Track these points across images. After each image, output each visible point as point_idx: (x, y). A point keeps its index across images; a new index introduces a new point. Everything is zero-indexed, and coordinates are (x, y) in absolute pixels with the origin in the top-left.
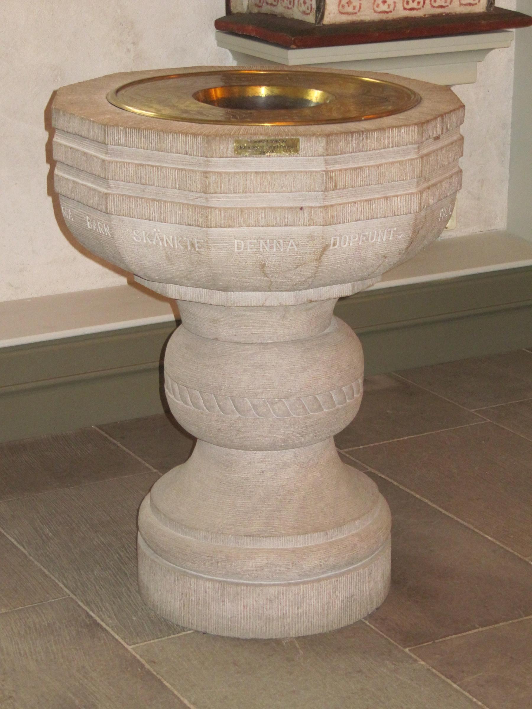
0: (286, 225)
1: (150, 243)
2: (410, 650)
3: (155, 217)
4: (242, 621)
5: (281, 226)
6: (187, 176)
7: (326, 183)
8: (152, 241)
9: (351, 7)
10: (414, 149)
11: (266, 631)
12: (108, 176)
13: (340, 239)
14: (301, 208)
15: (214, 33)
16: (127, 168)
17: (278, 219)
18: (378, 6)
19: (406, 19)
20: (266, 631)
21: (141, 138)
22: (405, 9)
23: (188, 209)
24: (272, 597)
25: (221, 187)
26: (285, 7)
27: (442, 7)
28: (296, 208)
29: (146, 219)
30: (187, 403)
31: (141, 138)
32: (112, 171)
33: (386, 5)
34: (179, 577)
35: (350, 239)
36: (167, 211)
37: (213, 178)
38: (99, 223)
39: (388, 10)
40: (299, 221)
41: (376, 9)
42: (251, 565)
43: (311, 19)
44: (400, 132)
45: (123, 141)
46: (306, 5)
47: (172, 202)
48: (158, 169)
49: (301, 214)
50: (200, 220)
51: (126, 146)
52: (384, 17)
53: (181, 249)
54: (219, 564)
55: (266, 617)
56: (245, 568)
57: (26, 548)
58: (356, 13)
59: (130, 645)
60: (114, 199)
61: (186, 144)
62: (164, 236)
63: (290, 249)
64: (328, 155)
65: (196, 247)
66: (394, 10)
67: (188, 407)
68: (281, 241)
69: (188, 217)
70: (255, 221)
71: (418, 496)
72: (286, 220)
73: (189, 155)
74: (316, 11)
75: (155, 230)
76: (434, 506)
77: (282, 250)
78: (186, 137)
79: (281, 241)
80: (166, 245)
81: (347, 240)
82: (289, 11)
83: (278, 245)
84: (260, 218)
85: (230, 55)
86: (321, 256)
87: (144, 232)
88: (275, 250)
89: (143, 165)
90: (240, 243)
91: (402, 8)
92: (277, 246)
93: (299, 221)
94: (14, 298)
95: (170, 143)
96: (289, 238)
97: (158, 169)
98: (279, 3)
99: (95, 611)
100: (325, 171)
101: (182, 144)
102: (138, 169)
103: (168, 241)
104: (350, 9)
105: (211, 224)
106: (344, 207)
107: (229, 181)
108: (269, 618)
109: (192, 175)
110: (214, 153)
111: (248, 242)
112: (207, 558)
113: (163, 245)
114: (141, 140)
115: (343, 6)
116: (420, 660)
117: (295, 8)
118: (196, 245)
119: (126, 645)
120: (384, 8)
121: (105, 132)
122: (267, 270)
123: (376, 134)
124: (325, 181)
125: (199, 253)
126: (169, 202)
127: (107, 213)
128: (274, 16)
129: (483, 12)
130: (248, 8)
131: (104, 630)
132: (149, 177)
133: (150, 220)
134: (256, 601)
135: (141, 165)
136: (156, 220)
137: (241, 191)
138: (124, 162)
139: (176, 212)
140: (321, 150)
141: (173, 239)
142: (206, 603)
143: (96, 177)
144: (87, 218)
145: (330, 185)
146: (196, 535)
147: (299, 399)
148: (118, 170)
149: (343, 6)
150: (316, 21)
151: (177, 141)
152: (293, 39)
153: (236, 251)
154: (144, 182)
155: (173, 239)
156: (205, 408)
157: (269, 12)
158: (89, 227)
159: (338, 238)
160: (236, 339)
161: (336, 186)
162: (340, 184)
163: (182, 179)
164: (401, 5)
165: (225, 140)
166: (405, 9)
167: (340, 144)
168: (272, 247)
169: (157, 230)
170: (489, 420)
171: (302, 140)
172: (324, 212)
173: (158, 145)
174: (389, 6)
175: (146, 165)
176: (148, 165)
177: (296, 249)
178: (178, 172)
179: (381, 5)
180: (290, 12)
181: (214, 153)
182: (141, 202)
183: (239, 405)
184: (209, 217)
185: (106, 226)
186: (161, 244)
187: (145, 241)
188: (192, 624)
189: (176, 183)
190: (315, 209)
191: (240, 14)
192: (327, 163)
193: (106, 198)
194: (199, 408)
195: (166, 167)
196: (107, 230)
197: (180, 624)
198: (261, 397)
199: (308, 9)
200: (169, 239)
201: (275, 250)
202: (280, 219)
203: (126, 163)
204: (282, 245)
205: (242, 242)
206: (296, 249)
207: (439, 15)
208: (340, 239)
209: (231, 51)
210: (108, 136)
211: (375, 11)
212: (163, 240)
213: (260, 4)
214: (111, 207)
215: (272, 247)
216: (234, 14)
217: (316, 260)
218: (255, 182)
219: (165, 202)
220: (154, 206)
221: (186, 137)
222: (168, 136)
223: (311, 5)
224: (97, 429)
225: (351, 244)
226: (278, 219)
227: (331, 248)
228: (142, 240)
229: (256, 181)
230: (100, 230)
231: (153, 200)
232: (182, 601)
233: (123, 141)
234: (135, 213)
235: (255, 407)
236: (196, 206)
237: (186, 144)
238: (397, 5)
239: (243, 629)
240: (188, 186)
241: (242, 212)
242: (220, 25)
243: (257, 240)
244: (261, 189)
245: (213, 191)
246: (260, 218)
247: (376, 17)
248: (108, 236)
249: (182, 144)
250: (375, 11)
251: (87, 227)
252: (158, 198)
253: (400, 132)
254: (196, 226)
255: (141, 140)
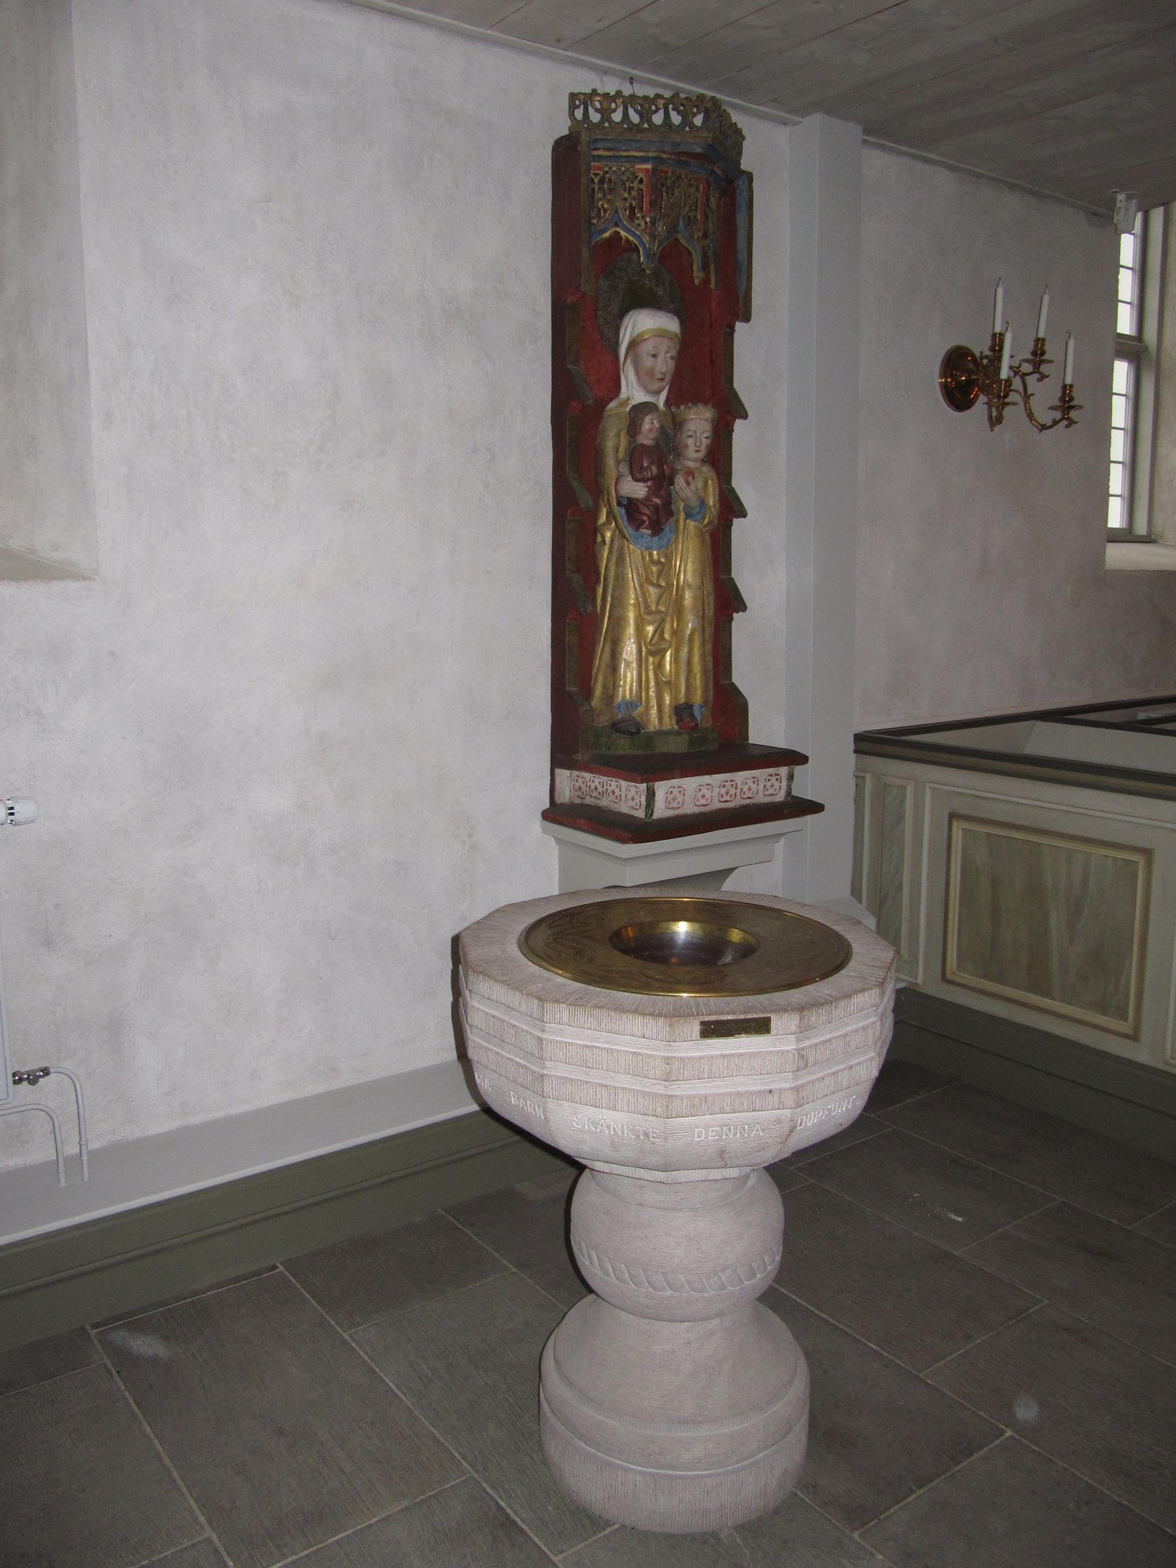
0: (753, 1111)
1: (594, 1129)
2: (859, 1536)
3: (602, 1103)
4: (677, 1516)
5: (748, 1112)
6: (644, 1061)
7: (798, 1063)
8: (596, 1128)
9: (676, 802)
10: (874, 1011)
11: (703, 1525)
12: (546, 1056)
13: (807, 1118)
14: (770, 1091)
15: (539, 822)
16: (569, 1049)
17: (746, 1104)
18: (698, 800)
19: (721, 810)
20: (703, 1525)
21: (588, 1017)
22: (720, 802)
23: (644, 1097)
24: (709, 1488)
25: (684, 1074)
26: (611, 801)
27: (750, 798)
28: (765, 1091)
29: (591, 1106)
30: (608, 1276)
31: (588, 1017)
32: (551, 1051)
33: (705, 799)
34: (603, 1467)
35: (815, 1116)
36: (618, 1098)
37: (676, 1065)
38: (528, 1102)
39: (706, 803)
40: (768, 1104)
41: (697, 803)
42: (687, 1456)
43: (640, 814)
44: (864, 996)
45: (565, 1019)
46: (635, 801)
47: (623, 1089)
48: (608, 1052)
49: (769, 1098)
50: (659, 1109)
51: (569, 1026)
52: (702, 809)
53: (631, 1138)
54: (652, 1457)
55: (703, 1509)
56: (681, 1460)
57: (408, 1395)
58: (680, 808)
59: (556, 1555)
60: (552, 1081)
61: (644, 1026)
62: (612, 1123)
63: (755, 1134)
64: (800, 1033)
65: (651, 1136)
66: (711, 803)
67: (609, 1279)
68: (746, 1126)
69: (644, 1106)
70: (720, 1108)
71: (783, 1290)
72: (754, 1105)
73: (647, 1038)
74: (646, 807)
75: (601, 1116)
76: (804, 1303)
77: (746, 1135)
78: (644, 1019)
79: (746, 1126)
80: (612, 1133)
81: (812, 1118)
82: (615, 805)
83: (742, 1131)
84: (725, 1105)
85: (553, 839)
86: (787, 1138)
87: (586, 1118)
88: (738, 1136)
89: (590, 1047)
90: (701, 1131)
91: (717, 801)
92: (741, 1132)
93: (768, 1104)
94: (357, 1082)
95: (624, 1025)
96: (755, 1123)
97: (608, 1052)
98: (604, 797)
99: (504, 1498)
100: (796, 1050)
101: (638, 1026)
102: (583, 1052)
103: (616, 1128)
104: (675, 805)
105: (671, 1114)
106: (813, 1085)
107: (693, 1067)
108: (707, 1512)
109: (649, 1060)
110: (678, 1037)
111: (711, 1129)
112: (637, 1450)
113: (610, 1132)
114: (588, 1020)
115: (669, 802)
116: (877, 1553)
117: (622, 803)
118: (651, 1135)
119: (552, 1556)
120: (703, 802)
121: (543, 1008)
122: (726, 1156)
123: (842, 1003)
124: (796, 1061)
125: (653, 1144)
126: (620, 1087)
127: (543, 1097)
128: (599, 808)
129: (783, 801)
130: (570, 799)
131: (521, 1530)
132: (596, 1061)
133: (596, 1107)
134: (692, 1494)
135: (586, 1046)
136: (604, 1106)
137: (706, 1076)
138: (566, 1043)
139: (629, 1100)
140: (793, 1028)
141: (622, 1127)
142: (636, 1497)
143: (528, 1055)
144: (512, 1093)
145: (802, 1064)
146: (621, 1420)
147: (735, 1270)
148: (558, 1051)
149: (669, 802)
150: (646, 816)
151: (632, 1022)
152: (631, 836)
153: (696, 1139)
154: (590, 1065)
155: (623, 1128)
156: (631, 1283)
157: (593, 804)
158: (513, 1102)
159: (804, 1117)
160: (663, 1205)
161: (807, 1064)
162: (811, 1060)
163: (637, 1065)
164: (717, 798)
165: (690, 1022)
166: (720, 802)
167: (812, 1018)
168: (735, 1134)
169: (603, 1116)
170: (812, 1181)
171: (773, 1017)
172: (795, 1093)
173: (609, 1027)
174: (707, 799)
175: (593, 1046)
176: (596, 1047)
177: (761, 1134)
178: (632, 1056)
179: (701, 799)
180: (616, 806)
181: (678, 1037)
182: (585, 1087)
183: (672, 1281)
184: (670, 1107)
185: (539, 1108)
186: (607, 1132)
187: (587, 1127)
188: (618, 1517)
189: (629, 1068)
190: (786, 1091)
191: (563, 804)
192: (798, 1040)
193: (542, 1081)
194: (624, 1282)
195: (618, 1051)
196: (540, 1112)
197: (603, 1516)
198: (696, 1272)
199: (637, 805)
200: (618, 1128)
201: (738, 1136)
202: (748, 1104)
203: (569, 1043)
204: (746, 1130)
205: (703, 1130)
206: (761, 1134)
207: (747, 806)
208: (807, 1118)
209: (555, 838)
210: (547, 1013)
211: (696, 805)
212: (610, 1127)
213: (583, 796)
214: (547, 1088)
215: (735, 1134)
216: (558, 805)
217: (781, 1143)
218: (721, 1066)
219: (615, 1088)
220: (602, 1091)
221: (644, 1019)
222: (622, 1017)
223: (640, 801)
224: (444, 1213)
225: (815, 1121)
226: (746, 1104)
227: (798, 1129)
228: (584, 1126)
229: (723, 1065)
230: (530, 1110)
231: (602, 1085)
232: (606, 1492)
233: (565, 1019)
234: (578, 1098)
235: (689, 1282)
236: (655, 1095)
237: (644, 1026)
238: (714, 798)
239: (678, 1525)
240: (645, 1072)
241: (706, 1099)
242: (547, 816)
243: (720, 1127)
244: (728, 1073)
245: (674, 1078)
246: (725, 1105)
247: (696, 810)
248: (540, 1117)
249: (638, 1026)
250: (696, 805)
251: (511, 1103)
252: (606, 1083)
253: (864, 996)
254: (653, 1116)
255: (588, 1020)
